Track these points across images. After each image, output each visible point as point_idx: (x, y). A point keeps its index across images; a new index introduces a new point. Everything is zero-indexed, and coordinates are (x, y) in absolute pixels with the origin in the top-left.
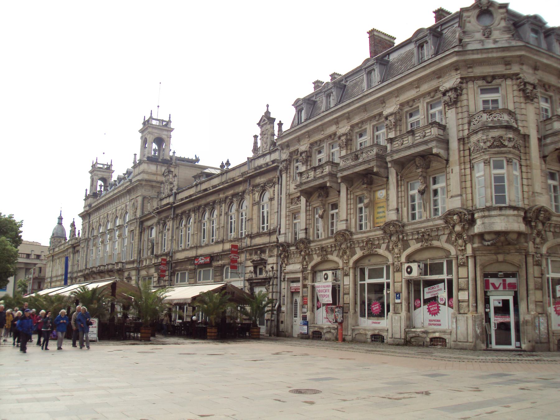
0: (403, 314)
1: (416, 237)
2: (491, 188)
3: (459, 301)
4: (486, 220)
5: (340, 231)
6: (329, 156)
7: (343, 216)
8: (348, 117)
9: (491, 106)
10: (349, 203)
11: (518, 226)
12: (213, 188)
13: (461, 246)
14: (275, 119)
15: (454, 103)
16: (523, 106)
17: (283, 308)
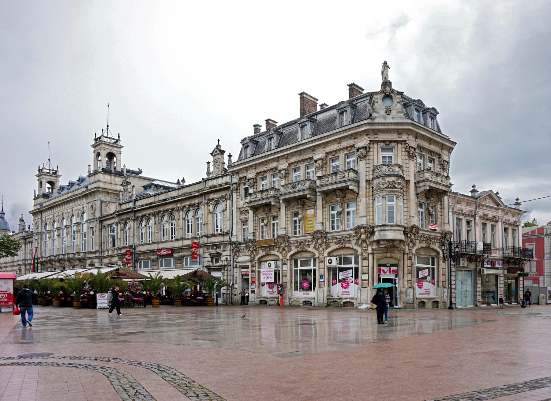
0: (326, 288)
1: (335, 241)
2: (386, 213)
3: (362, 280)
4: (382, 233)
5: (281, 235)
6: (271, 183)
7: (283, 225)
8: (287, 157)
9: (387, 160)
10: (287, 216)
11: (401, 236)
12: (172, 199)
13: (365, 248)
14: (224, 151)
15: (363, 157)
16: (407, 161)
17: (236, 286)
